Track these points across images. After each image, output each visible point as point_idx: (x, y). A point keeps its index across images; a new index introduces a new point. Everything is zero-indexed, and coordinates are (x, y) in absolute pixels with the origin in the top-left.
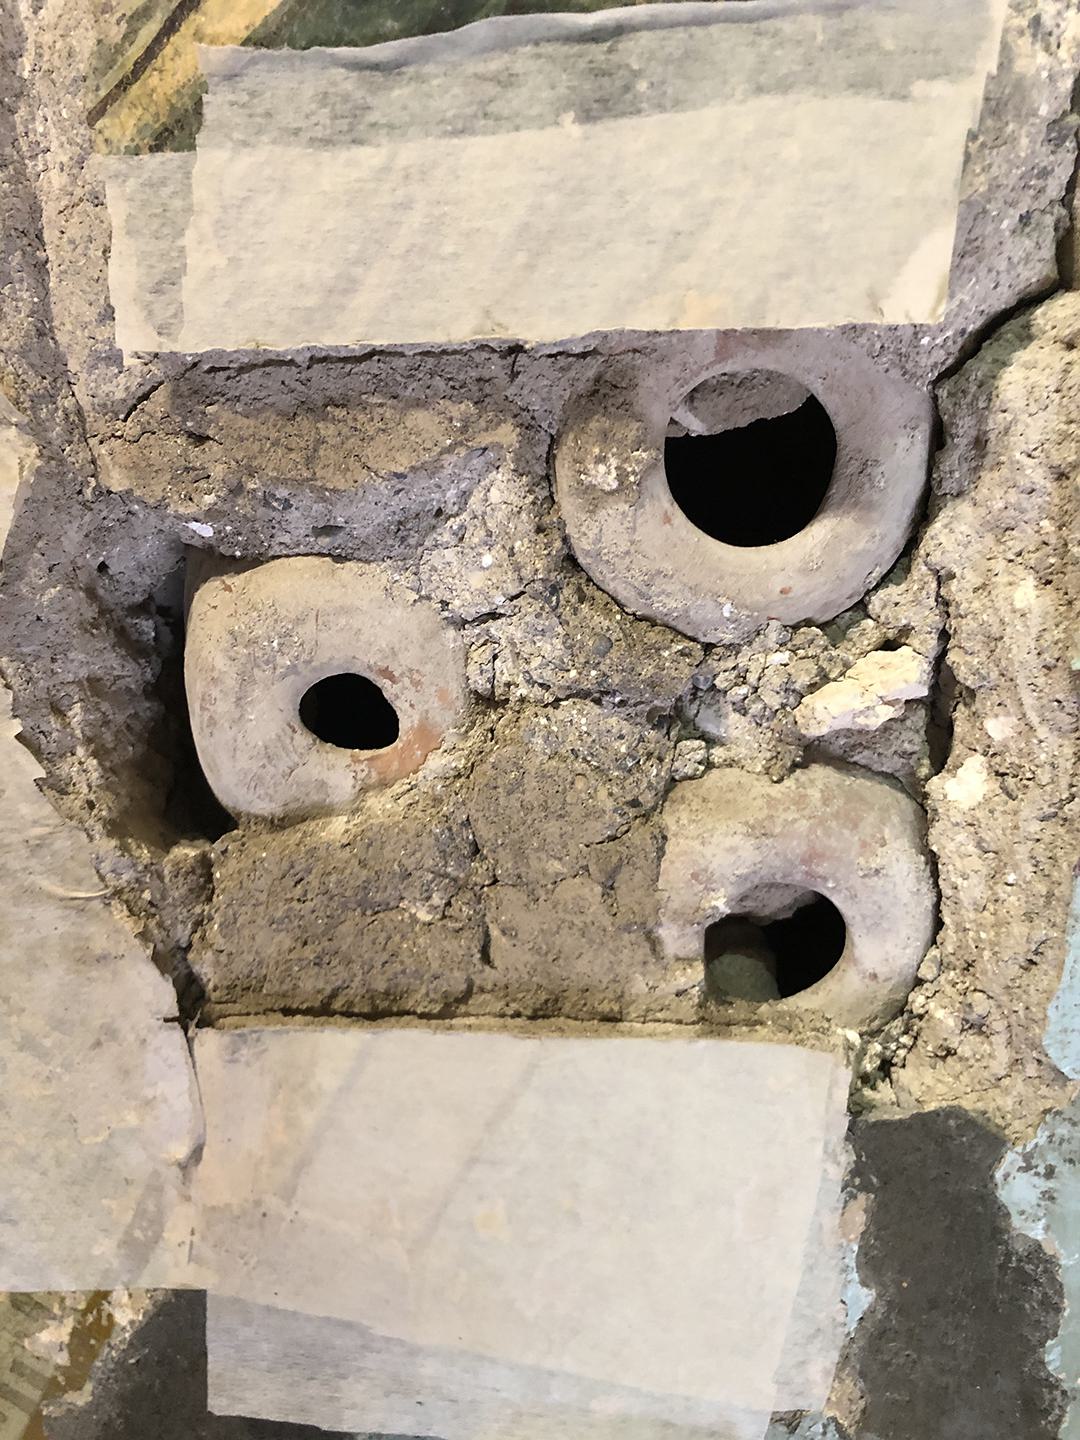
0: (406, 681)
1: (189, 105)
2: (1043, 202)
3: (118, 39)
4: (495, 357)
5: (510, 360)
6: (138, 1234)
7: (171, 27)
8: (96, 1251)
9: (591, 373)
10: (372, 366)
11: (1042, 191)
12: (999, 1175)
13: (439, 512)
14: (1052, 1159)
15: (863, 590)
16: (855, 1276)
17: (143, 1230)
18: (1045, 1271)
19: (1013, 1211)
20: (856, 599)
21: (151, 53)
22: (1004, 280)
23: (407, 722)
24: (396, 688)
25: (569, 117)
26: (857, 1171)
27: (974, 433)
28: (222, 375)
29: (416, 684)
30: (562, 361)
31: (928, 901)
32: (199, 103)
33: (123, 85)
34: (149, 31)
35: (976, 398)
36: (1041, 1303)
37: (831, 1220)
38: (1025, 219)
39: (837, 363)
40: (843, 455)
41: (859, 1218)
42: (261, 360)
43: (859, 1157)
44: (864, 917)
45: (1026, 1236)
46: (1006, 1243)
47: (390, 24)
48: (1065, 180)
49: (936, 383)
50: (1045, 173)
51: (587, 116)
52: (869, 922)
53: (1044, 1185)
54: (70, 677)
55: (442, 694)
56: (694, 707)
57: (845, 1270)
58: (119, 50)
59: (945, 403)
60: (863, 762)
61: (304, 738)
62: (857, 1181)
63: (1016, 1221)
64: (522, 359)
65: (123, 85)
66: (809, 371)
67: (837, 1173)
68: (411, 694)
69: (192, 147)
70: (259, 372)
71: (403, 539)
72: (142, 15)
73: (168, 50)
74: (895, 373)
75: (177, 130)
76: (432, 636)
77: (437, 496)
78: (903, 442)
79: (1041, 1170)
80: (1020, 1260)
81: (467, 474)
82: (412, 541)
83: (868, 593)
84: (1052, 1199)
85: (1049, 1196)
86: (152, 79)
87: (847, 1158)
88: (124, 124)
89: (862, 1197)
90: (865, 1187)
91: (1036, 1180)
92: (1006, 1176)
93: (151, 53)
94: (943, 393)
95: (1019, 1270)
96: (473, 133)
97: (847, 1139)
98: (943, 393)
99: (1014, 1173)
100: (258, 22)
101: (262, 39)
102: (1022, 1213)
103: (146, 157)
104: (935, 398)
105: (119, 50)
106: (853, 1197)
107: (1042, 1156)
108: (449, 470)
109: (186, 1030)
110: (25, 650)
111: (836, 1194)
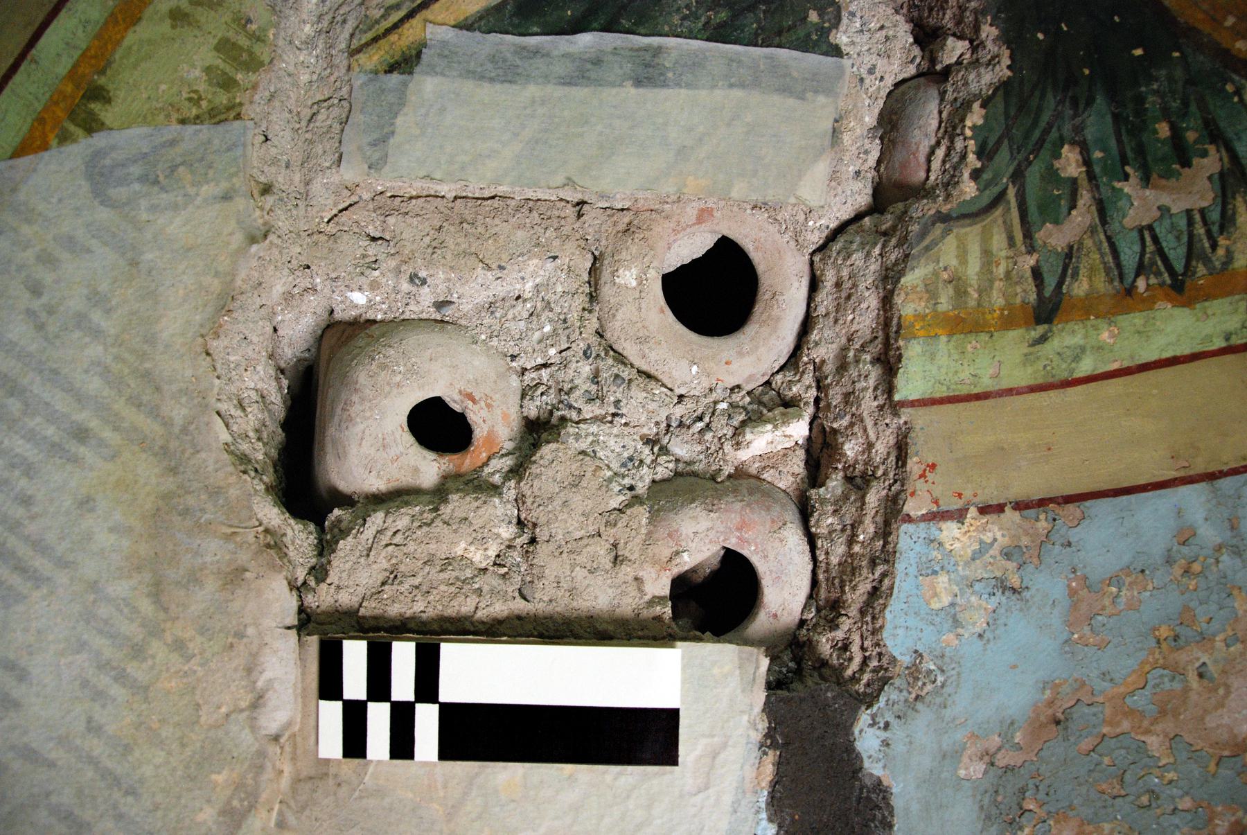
0: (483, 404)
1: (414, 52)
2: (866, 167)
3: (378, 16)
4: (569, 206)
5: (578, 208)
6: (235, 803)
7: (411, 15)
8: (201, 817)
9: (626, 220)
10: (496, 203)
11: (865, 161)
12: (856, 731)
13: (518, 297)
14: (889, 717)
15: (770, 373)
16: (764, 815)
17: (242, 800)
18: (884, 798)
19: (864, 756)
20: (766, 378)
21: (396, 26)
22: (850, 201)
23: (479, 433)
24: (476, 408)
25: (629, 83)
26: (770, 734)
27: (834, 279)
28: (399, 199)
29: (489, 406)
30: (609, 212)
31: (810, 567)
32: (419, 55)
33: (376, 40)
34: (395, 17)
35: (836, 259)
36: (881, 822)
37: (750, 773)
38: (858, 173)
39: (762, 234)
40: (762, 289)
41: (769, 770)
42: (425, 193)
43: (770, 723)
44: (771, 571)
45: (872, 774)
46: (860, 780)
47: (535, 29)
48: (876, 157)
49: (812, 254)
50: (866, 152)
51: (638, 83)
52: (774, 575)
53: (884, 735)
54: (252, 385)
55: (505, 416)
56: (667, 437)
57: (758, 812)
58: (377, 22)
59: (817, 265)
60: (769, 479)
61: (409, 438)
62: (769, 742)
63: (866, 764)
64: (586, 207)
65: (376, 40)
66: (746, 237)
67: (756, 736)
68: (484, 413)
69: (411, 73)
70: (423, 200)
71: (492, 313)
72: (397, 7)
73: (407, 25)
74: (793, 243)
75: (406, 63)
76: (501, 376)
77: (518, 286)
78: (796, 284)
79: (882, 725)
80: (868, 792)
81: (542, 273)
82: (498, 315)
83: (773, 375)
84: (888, 745)
85: (886, 743)
86: (393, 37)
87: (763, 725)
88: (373, 58)
89: (771, 752)
90: (773, 746)
91: (878, 732)
92: (861, 731)
93: (396, 26)
94: (817, 259)
95: (868, 799)
96: (576, 85)
97: (763, 711)
98: (817, 259)
99: (866, 729)
100: (462, 18)
101: (466, 26)
102: (870, 757)
103: (382, 76)
104: (812, 263)
105: (377, 22)
106: (765, 753)
107: (882, 715)
108: (531, 268)
109: (299, 635)
110: (232, 358)
111: (756, 753)
